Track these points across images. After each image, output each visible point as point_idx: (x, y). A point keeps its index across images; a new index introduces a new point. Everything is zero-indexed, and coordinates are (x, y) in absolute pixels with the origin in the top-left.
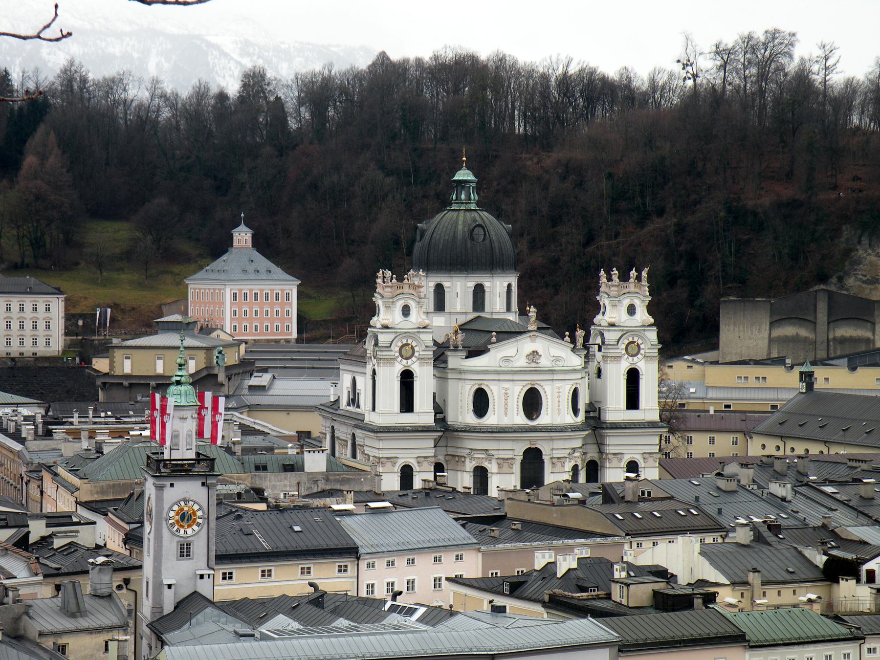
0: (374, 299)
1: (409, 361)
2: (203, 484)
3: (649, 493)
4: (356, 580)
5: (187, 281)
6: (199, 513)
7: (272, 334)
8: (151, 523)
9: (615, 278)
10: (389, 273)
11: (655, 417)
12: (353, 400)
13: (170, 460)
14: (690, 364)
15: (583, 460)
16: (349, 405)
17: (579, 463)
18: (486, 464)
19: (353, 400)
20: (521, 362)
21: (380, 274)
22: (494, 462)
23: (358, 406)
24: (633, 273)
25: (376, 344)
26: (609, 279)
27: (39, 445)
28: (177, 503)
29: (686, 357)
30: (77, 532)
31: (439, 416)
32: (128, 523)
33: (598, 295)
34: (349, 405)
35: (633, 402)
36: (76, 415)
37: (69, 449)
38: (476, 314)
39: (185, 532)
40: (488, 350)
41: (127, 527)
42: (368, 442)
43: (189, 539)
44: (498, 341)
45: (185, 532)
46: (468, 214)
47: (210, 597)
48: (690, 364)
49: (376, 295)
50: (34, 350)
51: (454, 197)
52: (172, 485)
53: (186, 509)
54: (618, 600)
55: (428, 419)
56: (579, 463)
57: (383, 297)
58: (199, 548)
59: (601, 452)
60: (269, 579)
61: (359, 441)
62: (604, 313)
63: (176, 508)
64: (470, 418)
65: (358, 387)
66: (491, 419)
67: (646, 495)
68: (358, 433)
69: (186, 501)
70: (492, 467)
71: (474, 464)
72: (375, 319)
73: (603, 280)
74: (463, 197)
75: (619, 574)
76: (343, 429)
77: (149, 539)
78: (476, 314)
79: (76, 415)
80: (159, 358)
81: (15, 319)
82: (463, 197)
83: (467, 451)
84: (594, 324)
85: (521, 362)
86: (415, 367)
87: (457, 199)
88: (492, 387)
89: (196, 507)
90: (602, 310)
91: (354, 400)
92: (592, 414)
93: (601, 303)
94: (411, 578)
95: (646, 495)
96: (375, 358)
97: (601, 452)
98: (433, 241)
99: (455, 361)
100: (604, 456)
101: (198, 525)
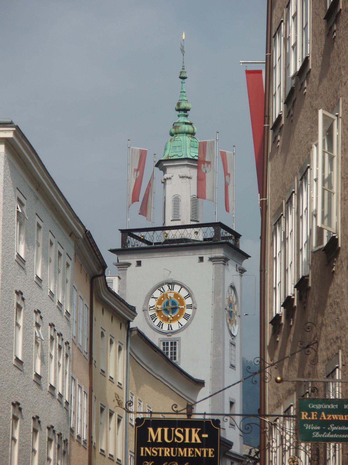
6: (188, 301)
28: (159, 287)
39: (170, 327)
43: (174, 336)
45: (170, 327)
52: (139, 263)
63: (157, 294)
69: (171, 284)
89: (184, 293)
101: (187, 317)
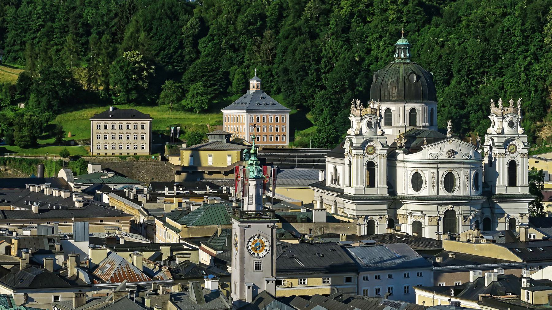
0: (349, 118)
1: (372, 156)
2: (268, 226)
3: (534, 237)
4: (356, 287)
5: (222, 111)
7: (273, 142)
8: (237, 249)
9: (500, 103)
10: (358, 102)
11: (527, 191)
12: (335, 181)
13: (248, 211)
14: (537, 160)
15: (481, 218)
16: (332, 183)
17: (479, 219)
18: (421, 220)
19: (335, 181)
20: (444, 157)
21: (352, 102)
22: (427, 218)
23: (339, 184)
24: (511, 102)
25: (351, 145)
26: (497, 105)
27: (150, 206)
29: (534, 156)
30: (190, 254)
31: (391, 190)
32: (216, 250)
33: (490, 115)
34: (332, 183)
35: (512, 182)
36: (166, 189)
37: (167, 208)
38: (412, 127)
40: (422, 149)
41: (215, 252)
42: (346, 205)
44: (427, 144)
46: (406, 66)
47: (273, 294)
48: (537, 160)
49: (351, 115)
50: (135, 151)
51: (397, 56)
53: (258, 241)
54: (526, 301)
55: (384, 192)
56: (479, 219)
57: (355, 116)
58: (267, 264)
59: (493, 213)
60: (304, 285)
61: (339, 205)
62: (493, 127)
64: (411, 192)
65: (338, 172)
66: (424, 192)
67: (532, 238)
68: (339, 200)
70: (425, 221)
71: (413, 219)
72: (350, 130)
73: (492, 105)
74: (402, 55)
75: (524, 283)
76: (328, 197)
77: (236, 259)
78: (412, 127)
79: (166, 189)
80: (210, 156)
81: (125, 133)
82: (402, 55)
83: (409, 212)
84: (487, 134)
85: (444, 157)
86: (377, 160)
87: (398, 56)
88: (424, 172)
89: (264, 240)
90: (492, 124)
91: (335, 180)
92: (486, 189)
93: (492, 120)
94: (390, 286)
95: (532, 238)
96: (350, 154)
97: (493, 213)
98: (384, 82)
99: (401, 156)
100: (495, 215)
101: (266, 250)
